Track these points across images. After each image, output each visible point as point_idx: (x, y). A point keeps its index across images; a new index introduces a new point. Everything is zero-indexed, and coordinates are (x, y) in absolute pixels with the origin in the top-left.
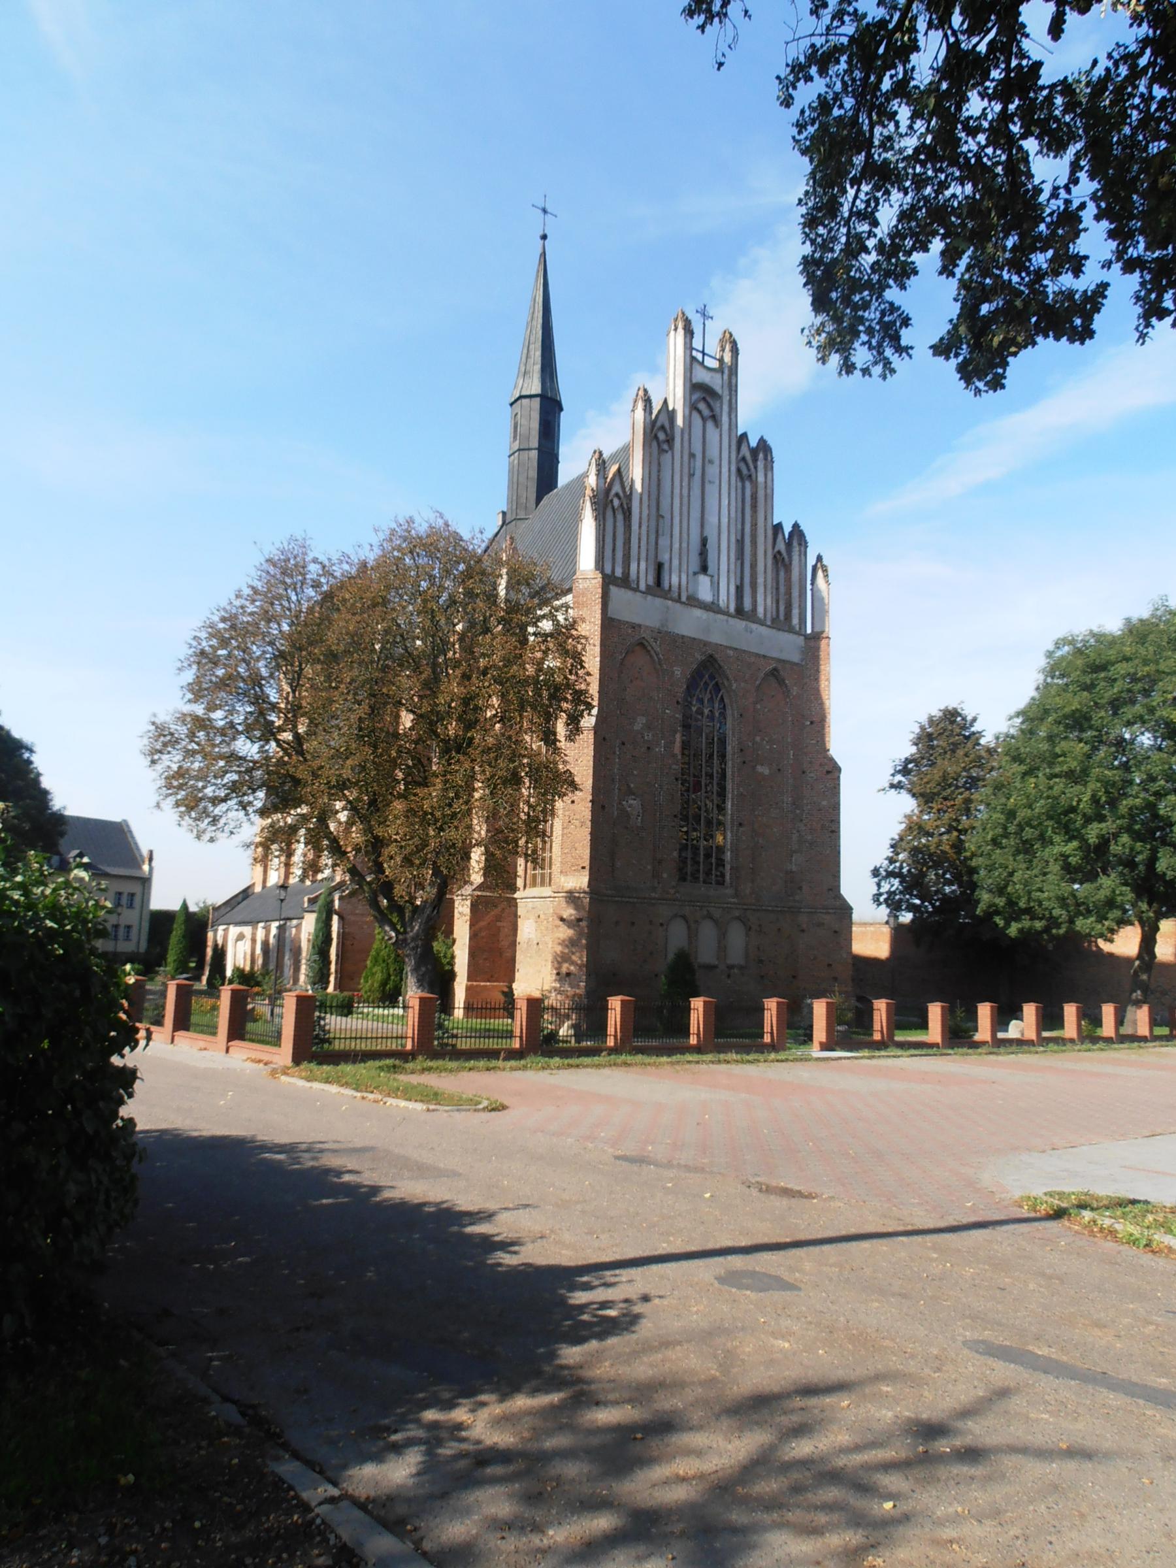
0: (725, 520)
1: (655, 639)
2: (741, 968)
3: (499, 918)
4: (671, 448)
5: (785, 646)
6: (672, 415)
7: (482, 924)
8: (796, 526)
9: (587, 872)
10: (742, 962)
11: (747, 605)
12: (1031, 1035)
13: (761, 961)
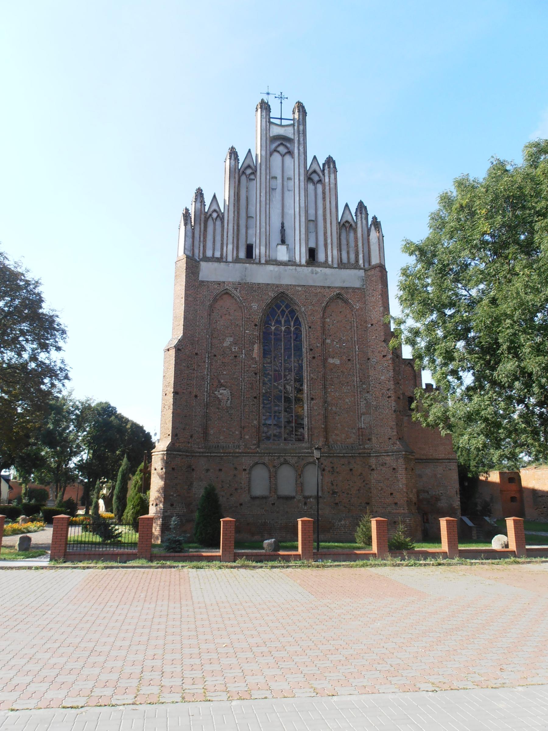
0: (297, 210)
1: (236, 289)
4: (256, 176)
5: (351, 278)
8: (361, 204)
9: (170, 438)
12: (513, 547)
13: (334, 493)
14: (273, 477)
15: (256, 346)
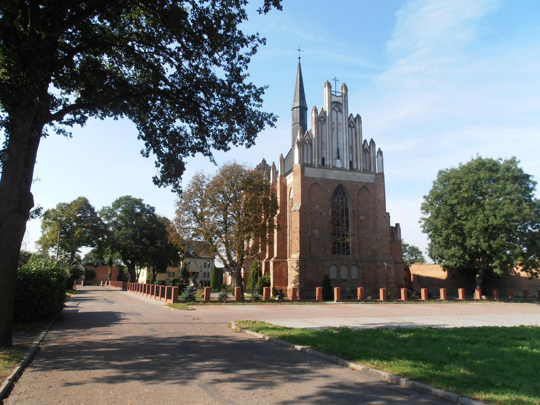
0: (345, 142)
1: (321, 181)
2: (356, 280)
3: (282, 267)
4: (325, 122)
5: (368, 178)
6: (325, 113)
7: (277, 269)
8: (372, 140)
10: (357, 278)
11: (355, 166)
14: (338, 271)
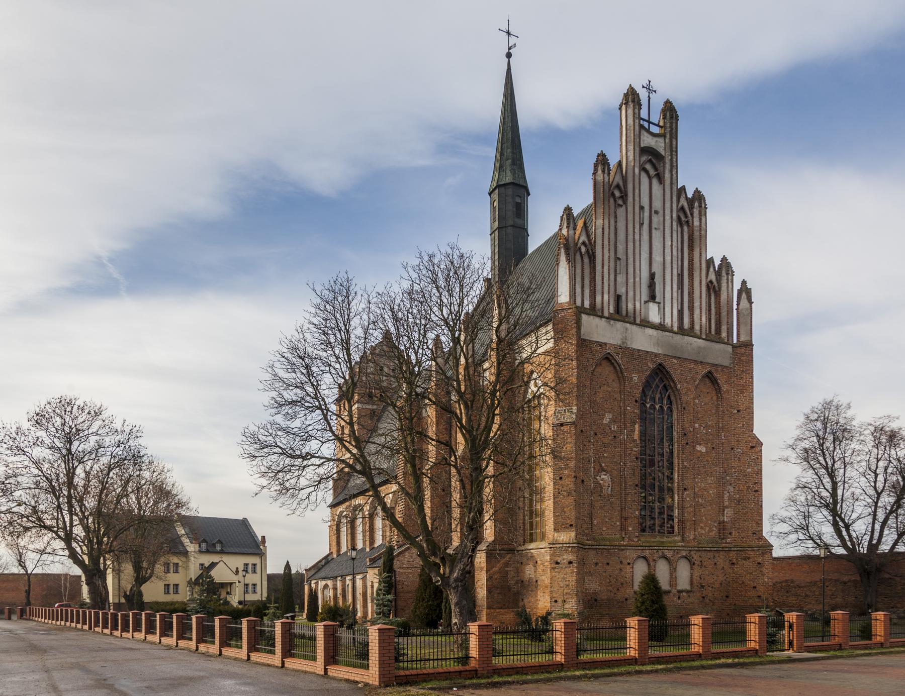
0: (668, 258)
5: (720, 354)
15: (637, 426)
